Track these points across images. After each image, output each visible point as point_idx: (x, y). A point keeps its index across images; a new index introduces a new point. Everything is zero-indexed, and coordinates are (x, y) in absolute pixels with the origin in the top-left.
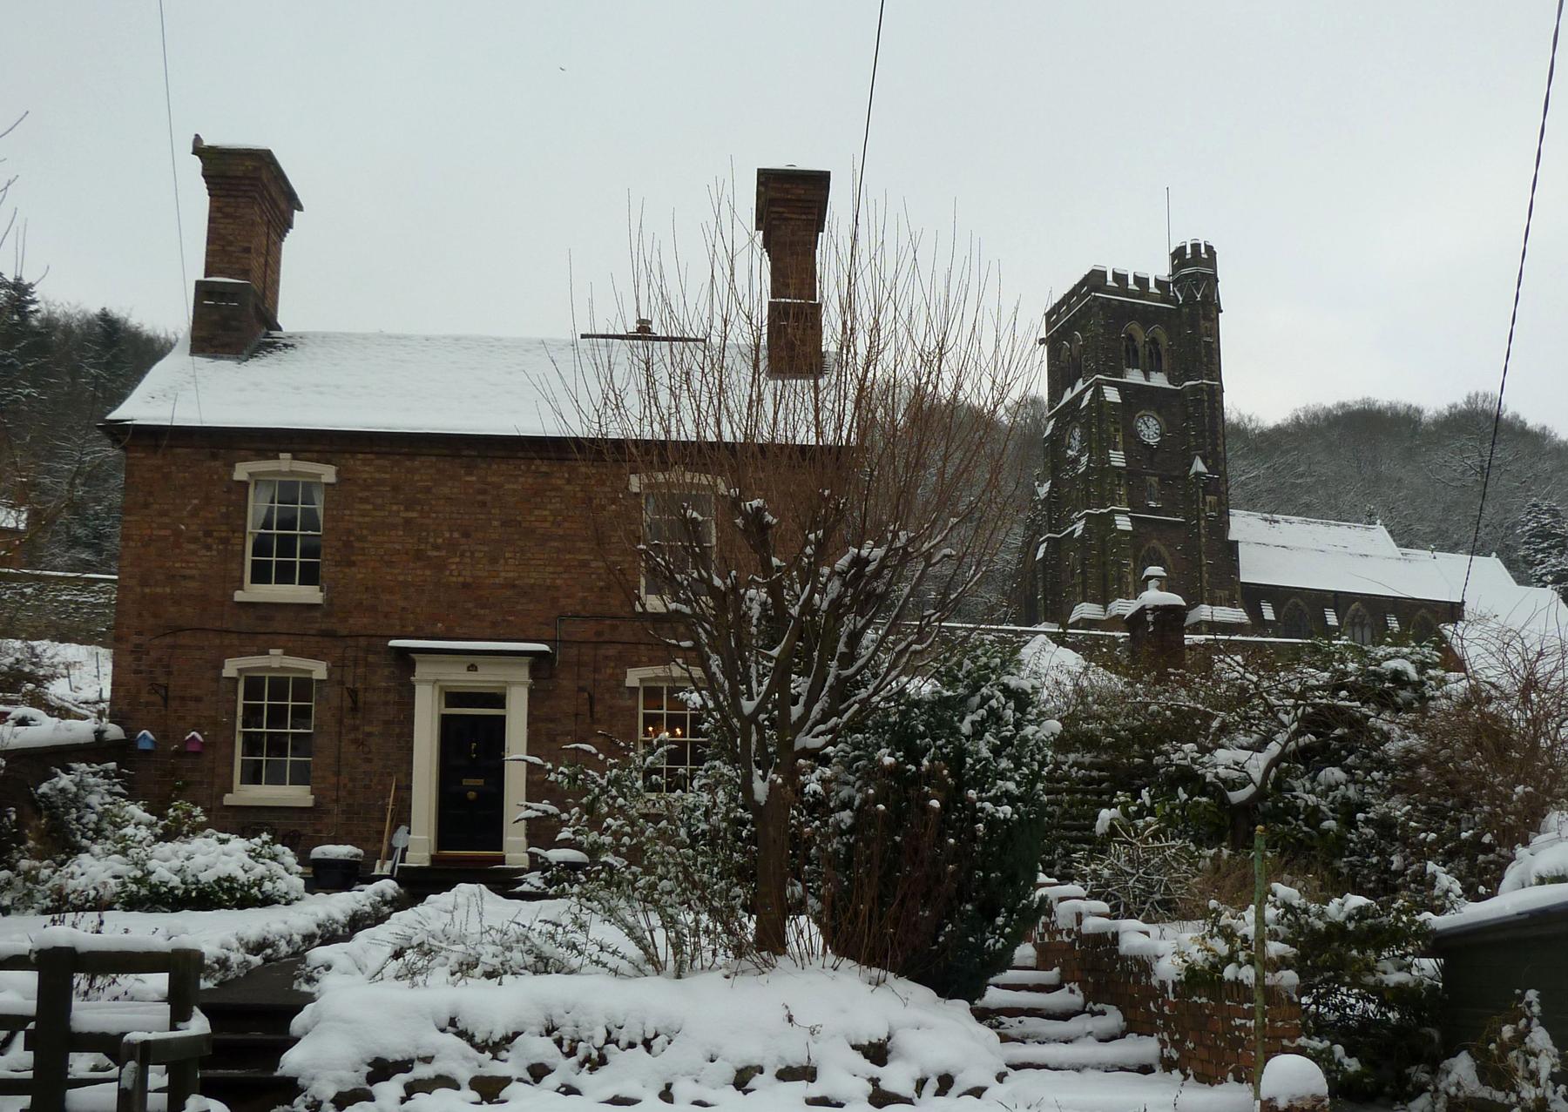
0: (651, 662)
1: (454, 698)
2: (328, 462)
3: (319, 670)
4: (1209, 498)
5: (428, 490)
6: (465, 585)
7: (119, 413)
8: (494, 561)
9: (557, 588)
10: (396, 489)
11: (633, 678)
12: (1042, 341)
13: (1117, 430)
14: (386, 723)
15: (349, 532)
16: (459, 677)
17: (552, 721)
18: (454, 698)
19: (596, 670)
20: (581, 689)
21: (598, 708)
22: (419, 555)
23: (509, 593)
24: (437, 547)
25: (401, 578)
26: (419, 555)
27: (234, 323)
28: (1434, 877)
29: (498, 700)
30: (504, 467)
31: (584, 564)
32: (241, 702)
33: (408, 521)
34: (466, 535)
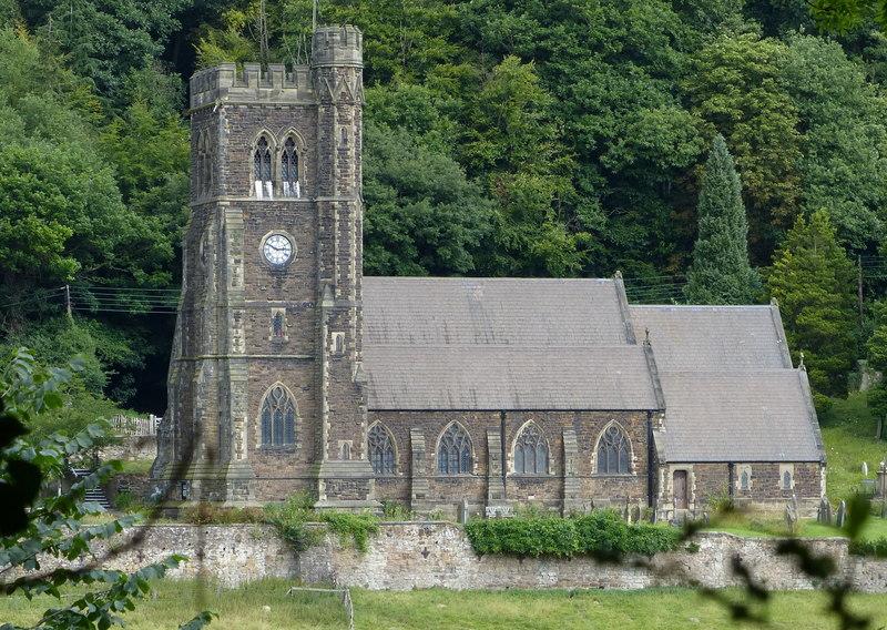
4: (334, 335)
13: (237, 262)
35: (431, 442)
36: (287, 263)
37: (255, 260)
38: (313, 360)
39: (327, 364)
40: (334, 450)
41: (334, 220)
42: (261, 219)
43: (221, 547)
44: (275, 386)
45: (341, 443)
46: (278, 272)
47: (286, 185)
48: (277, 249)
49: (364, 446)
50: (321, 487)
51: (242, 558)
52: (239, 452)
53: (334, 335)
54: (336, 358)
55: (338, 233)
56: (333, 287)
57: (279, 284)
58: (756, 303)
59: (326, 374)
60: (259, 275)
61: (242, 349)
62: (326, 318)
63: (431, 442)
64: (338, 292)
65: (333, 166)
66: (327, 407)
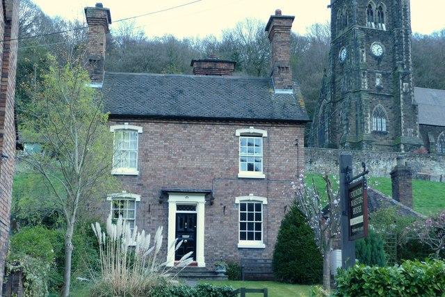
0: (243, 195)
1: (179, 207)
2: (140, 125)
3: (138, 198)
4: (404, 84)
5: (172, 135)
6: (184, 168)
7: (362, 216)
8: (193, 160)
9: (213, 169)
10: (161, 135)
11: (238, 200)
12: (329, 6)
13: (363, 51)
14: (159, 216)
15: (147, 150)
16: (183, 199)
17: (212, 215)
18: (179, 207)
19: (226, 198)
20: (221, 204)
21: (226, 211)
22: (169, 158)
23: (198, 171)
24: (175, 155)
25: (164, 166)
26: (169, 158)
27: (98, 71)
28: (162, 277)
29: (193, 207)
30: (196, 127)
31: (221, 161)
32: (262, 231)
33: (165, 146)
34: (184, 151)
35: (436, 139)
36: (381, 56)
37: (370, 54)
38: (395, 95)
39: (402, 96)
40: (406, 132)
41: (402, 37)
42: (372, 36)
43: (372, 162)
44: (378, 106)
45: (408, 130)
46: (379, 59)
47: (380, 24)
48: (377, 49)
49: (418, 132)
50: (402, 147)
51: (382, 167)
52: (367, 130)
53: (404, 84)
54: (405, 94)
55: (404, 42)
56: (403, 65)
57: (378, 64)
58: (168, 225)
59: (402, 100)
60: (371, 59)
61: (366, 87)
62: (401, 77)
63: (436, 139)
64: (405, 67)
65: (244, 259)
66: (402, 114)
